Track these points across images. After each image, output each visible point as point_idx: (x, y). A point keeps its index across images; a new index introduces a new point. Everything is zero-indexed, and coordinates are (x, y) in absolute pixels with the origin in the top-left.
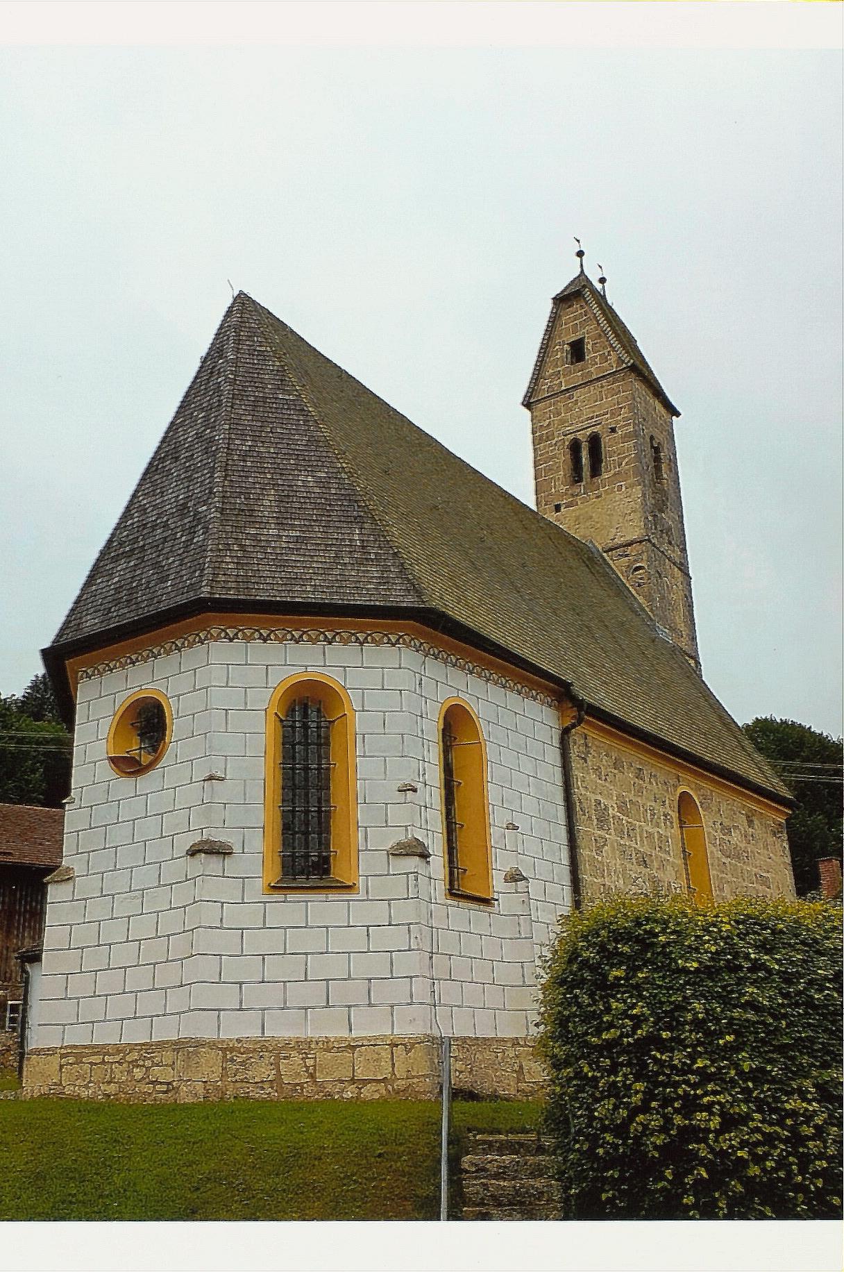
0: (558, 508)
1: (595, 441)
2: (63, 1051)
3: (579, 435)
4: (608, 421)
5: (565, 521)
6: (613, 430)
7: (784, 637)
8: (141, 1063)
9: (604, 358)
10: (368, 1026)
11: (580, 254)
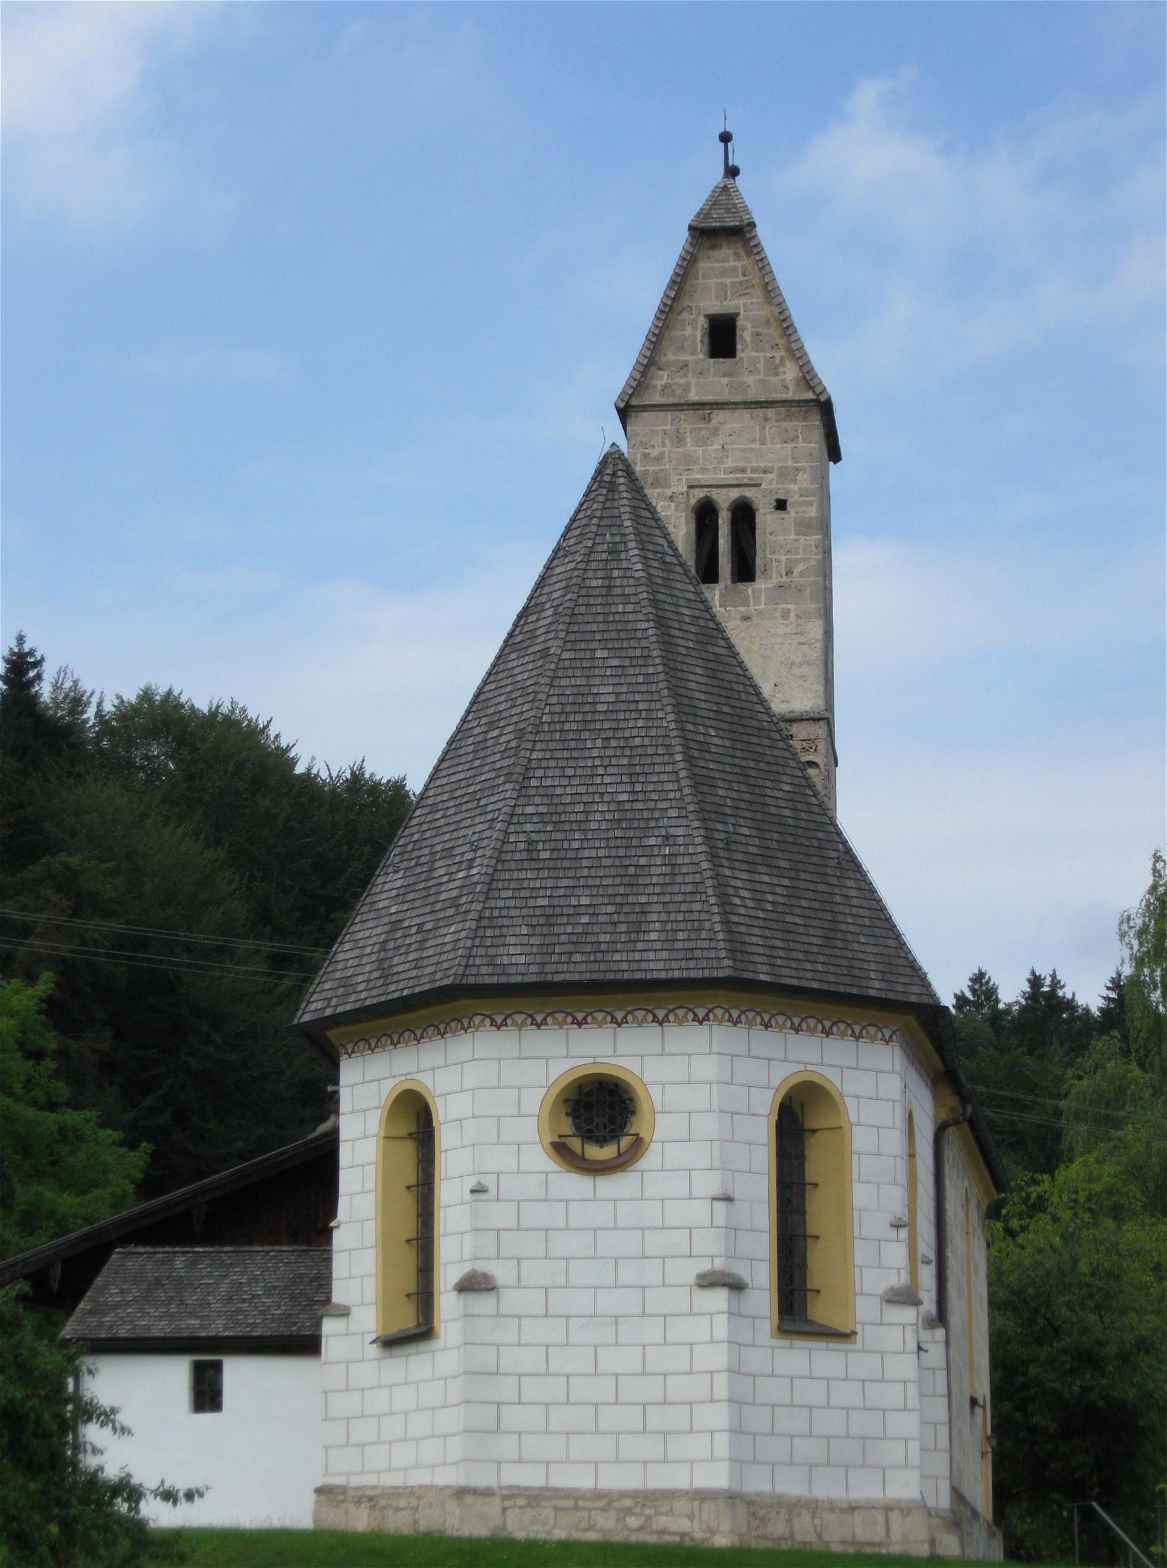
1: (744, 514)
3: (716, 494)
4: (772, 485)
7: (989, 865)
8: (638, 1510)
9: (774, 368)
10: (865, 1489)
11: (726, 138)
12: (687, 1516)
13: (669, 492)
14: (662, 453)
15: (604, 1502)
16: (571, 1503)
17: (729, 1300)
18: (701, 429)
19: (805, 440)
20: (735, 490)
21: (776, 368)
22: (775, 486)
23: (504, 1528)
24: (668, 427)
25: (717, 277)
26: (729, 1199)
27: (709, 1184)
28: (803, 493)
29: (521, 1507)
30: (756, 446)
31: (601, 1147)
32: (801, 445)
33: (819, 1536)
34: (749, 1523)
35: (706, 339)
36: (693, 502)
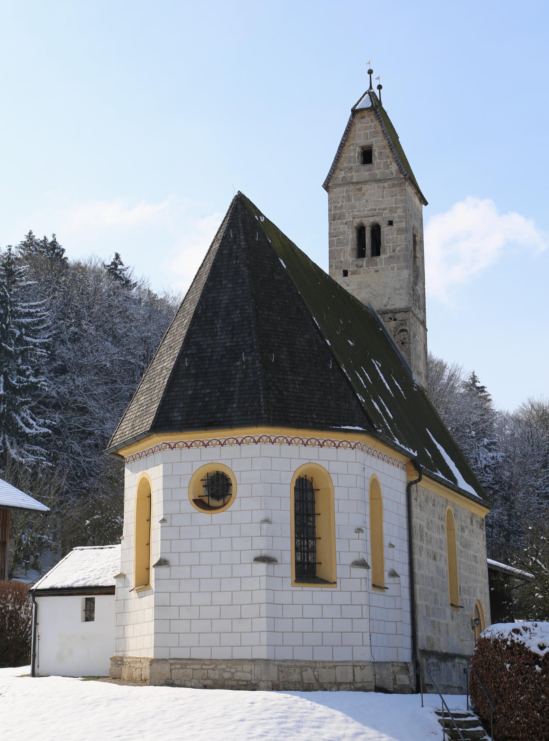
0: (345, 273)
1: (376, 229)
2: (171, 661)
4: (387, 215)
5: (350, 285)
6: (391, 223)
8: (228, 670)
9: (387, 166)
11: (370, 72)
12: (249, 672)
13: (345, 221)
14: (342, 205)
15: (214, 666)
16: (200, 666)
17: (267, 570)
18: (358, 194)
19: (400, 196)
20: (372, 218)
21: (388, 166)
22: (388, 215)
23: (171, 679)
24: (345, 194)
25: (364, 130)
26: (267, 521)
27: (259, 516)
28: (399, 217)
29: (179, 669)
30: (381, 199)
31: (218, 500)
32: (398, 197)
33: (317, 680)
34: (278, 675)
35: (360, 157)
36: (355, 224)
